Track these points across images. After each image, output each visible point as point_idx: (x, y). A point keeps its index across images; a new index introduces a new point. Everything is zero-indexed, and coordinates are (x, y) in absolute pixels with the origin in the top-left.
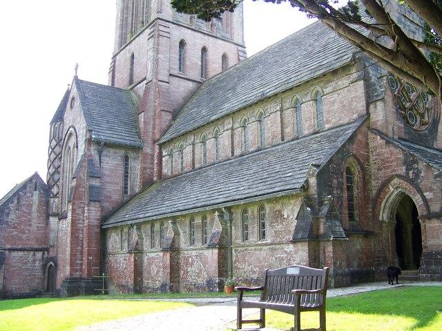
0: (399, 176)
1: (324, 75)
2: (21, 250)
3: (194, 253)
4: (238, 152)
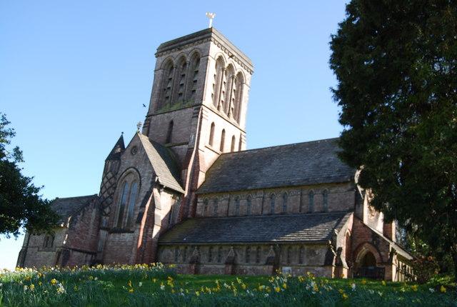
0: (368, 242)
1: (332, 183)
2: (80, 251)
3: (248, 267)
4: (266, 212)
